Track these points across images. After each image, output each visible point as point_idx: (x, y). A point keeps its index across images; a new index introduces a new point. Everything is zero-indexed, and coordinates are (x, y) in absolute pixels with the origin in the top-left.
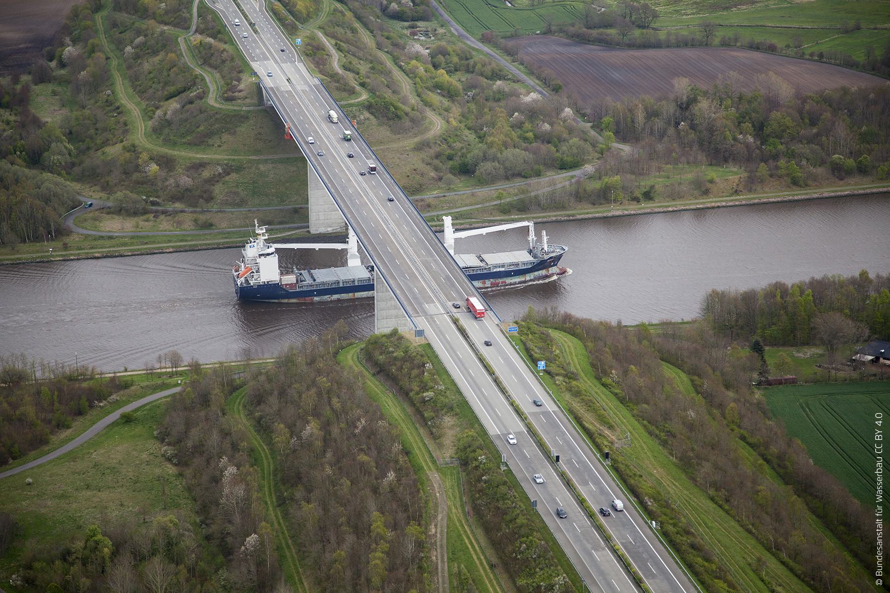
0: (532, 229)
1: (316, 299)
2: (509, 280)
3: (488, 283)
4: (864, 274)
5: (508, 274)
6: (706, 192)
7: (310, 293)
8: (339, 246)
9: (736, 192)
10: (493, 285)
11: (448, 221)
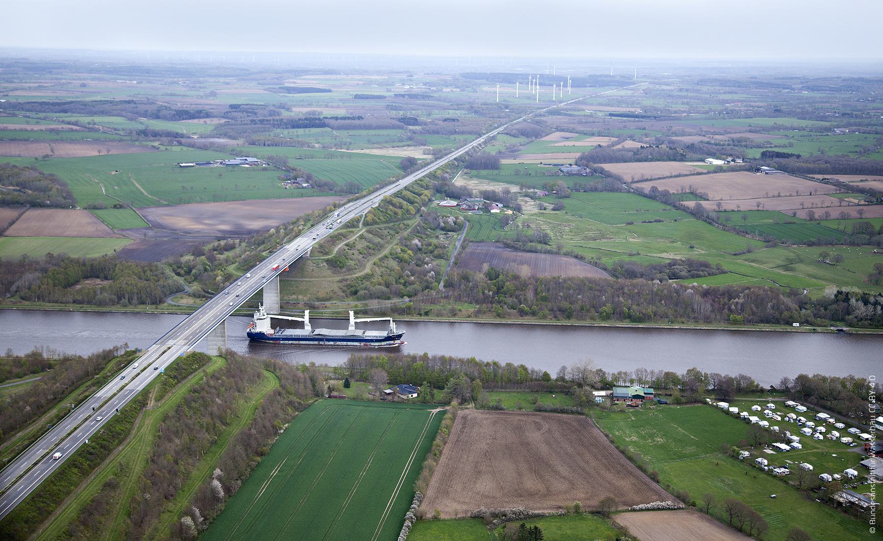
0: (391, 322)
1: (281, 342)
2: (372, 344)
3: (362, 344)
4: (425, 355)
5: (372, 341)
6: (455, 315)
7: (279, 339)
8: (300, 319)
9: (469, 317)
10: (365, 345)
11: (352, 313)
